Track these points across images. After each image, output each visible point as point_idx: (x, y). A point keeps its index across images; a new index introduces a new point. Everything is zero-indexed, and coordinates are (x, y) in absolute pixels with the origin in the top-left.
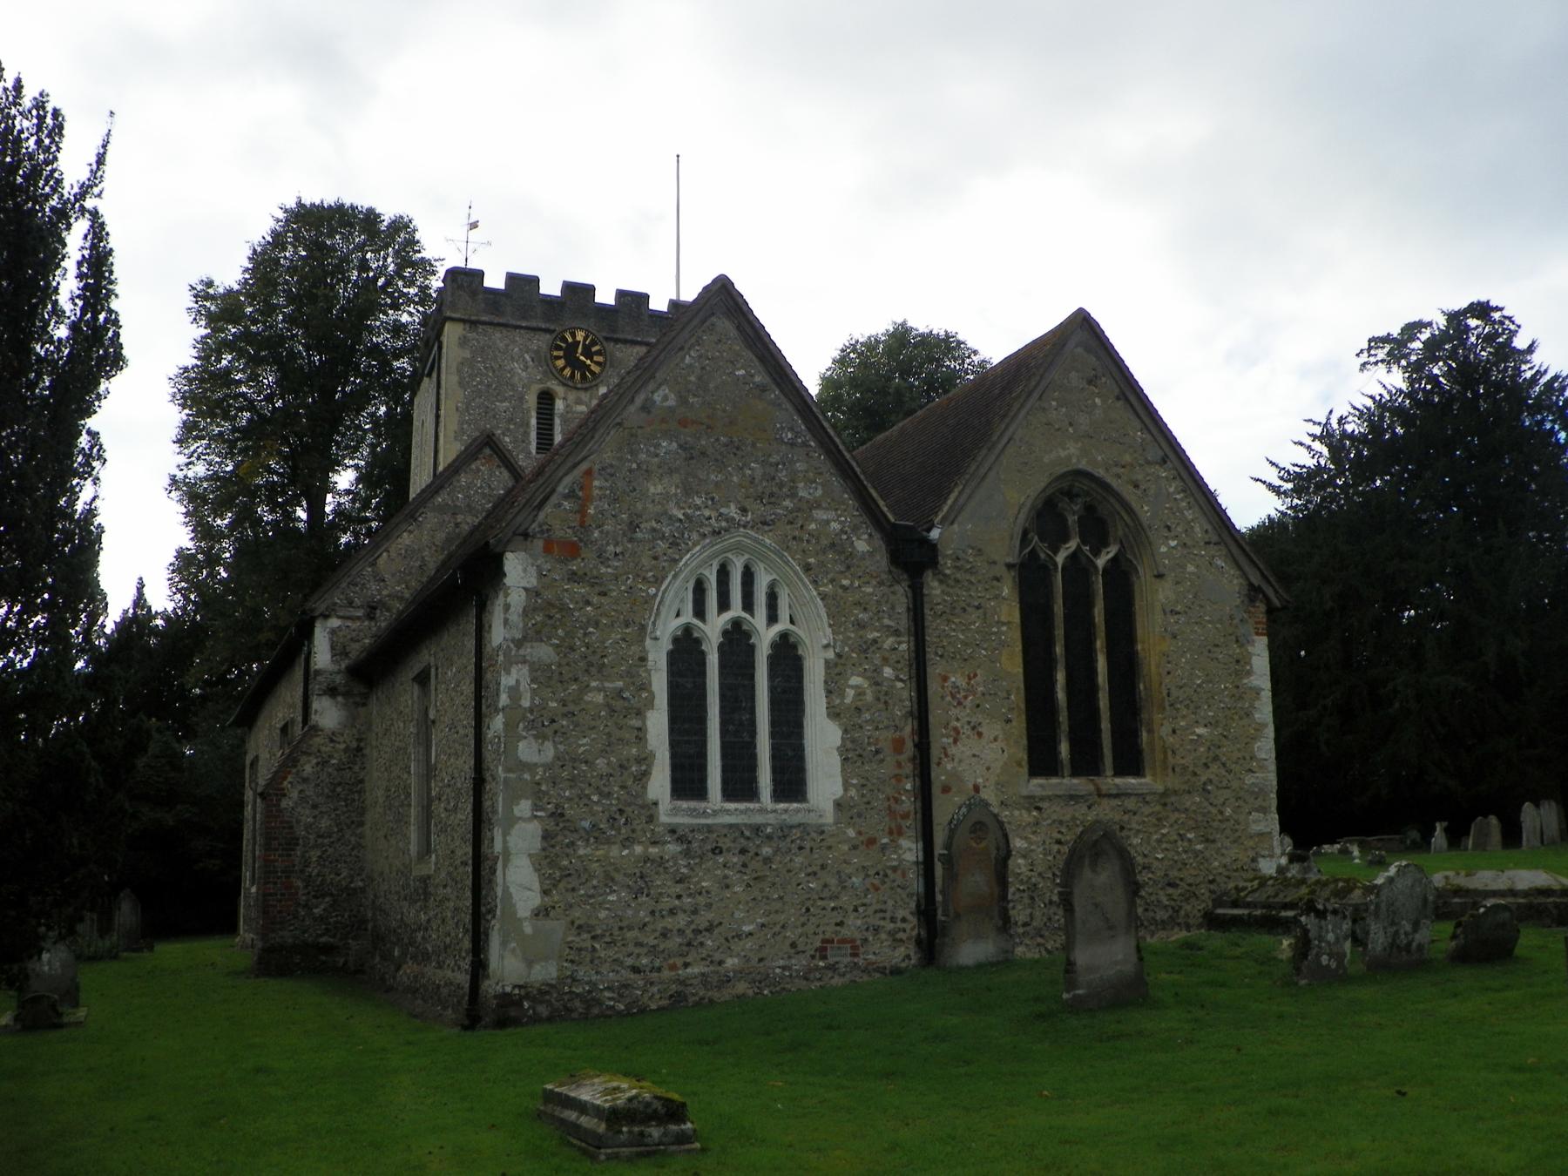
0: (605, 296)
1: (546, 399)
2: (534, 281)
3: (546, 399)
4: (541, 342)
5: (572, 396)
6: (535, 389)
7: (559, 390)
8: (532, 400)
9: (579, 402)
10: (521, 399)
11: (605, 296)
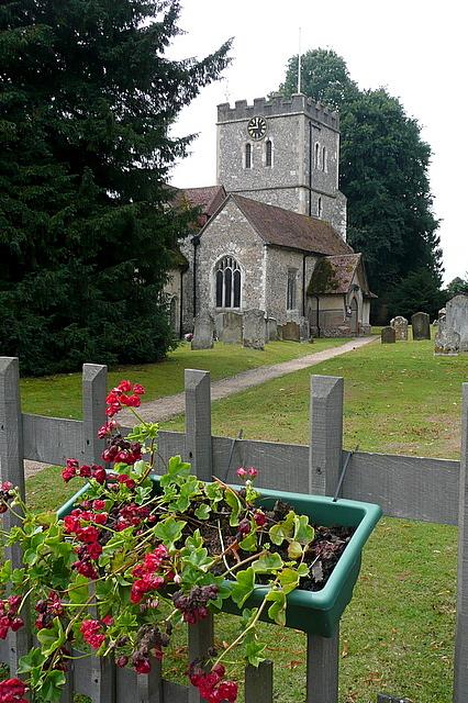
0: (250, 103)
1: (248, 146)
2: (245, 102)
3: (248, 146)
8: (243, 148)
11: (250, 103)
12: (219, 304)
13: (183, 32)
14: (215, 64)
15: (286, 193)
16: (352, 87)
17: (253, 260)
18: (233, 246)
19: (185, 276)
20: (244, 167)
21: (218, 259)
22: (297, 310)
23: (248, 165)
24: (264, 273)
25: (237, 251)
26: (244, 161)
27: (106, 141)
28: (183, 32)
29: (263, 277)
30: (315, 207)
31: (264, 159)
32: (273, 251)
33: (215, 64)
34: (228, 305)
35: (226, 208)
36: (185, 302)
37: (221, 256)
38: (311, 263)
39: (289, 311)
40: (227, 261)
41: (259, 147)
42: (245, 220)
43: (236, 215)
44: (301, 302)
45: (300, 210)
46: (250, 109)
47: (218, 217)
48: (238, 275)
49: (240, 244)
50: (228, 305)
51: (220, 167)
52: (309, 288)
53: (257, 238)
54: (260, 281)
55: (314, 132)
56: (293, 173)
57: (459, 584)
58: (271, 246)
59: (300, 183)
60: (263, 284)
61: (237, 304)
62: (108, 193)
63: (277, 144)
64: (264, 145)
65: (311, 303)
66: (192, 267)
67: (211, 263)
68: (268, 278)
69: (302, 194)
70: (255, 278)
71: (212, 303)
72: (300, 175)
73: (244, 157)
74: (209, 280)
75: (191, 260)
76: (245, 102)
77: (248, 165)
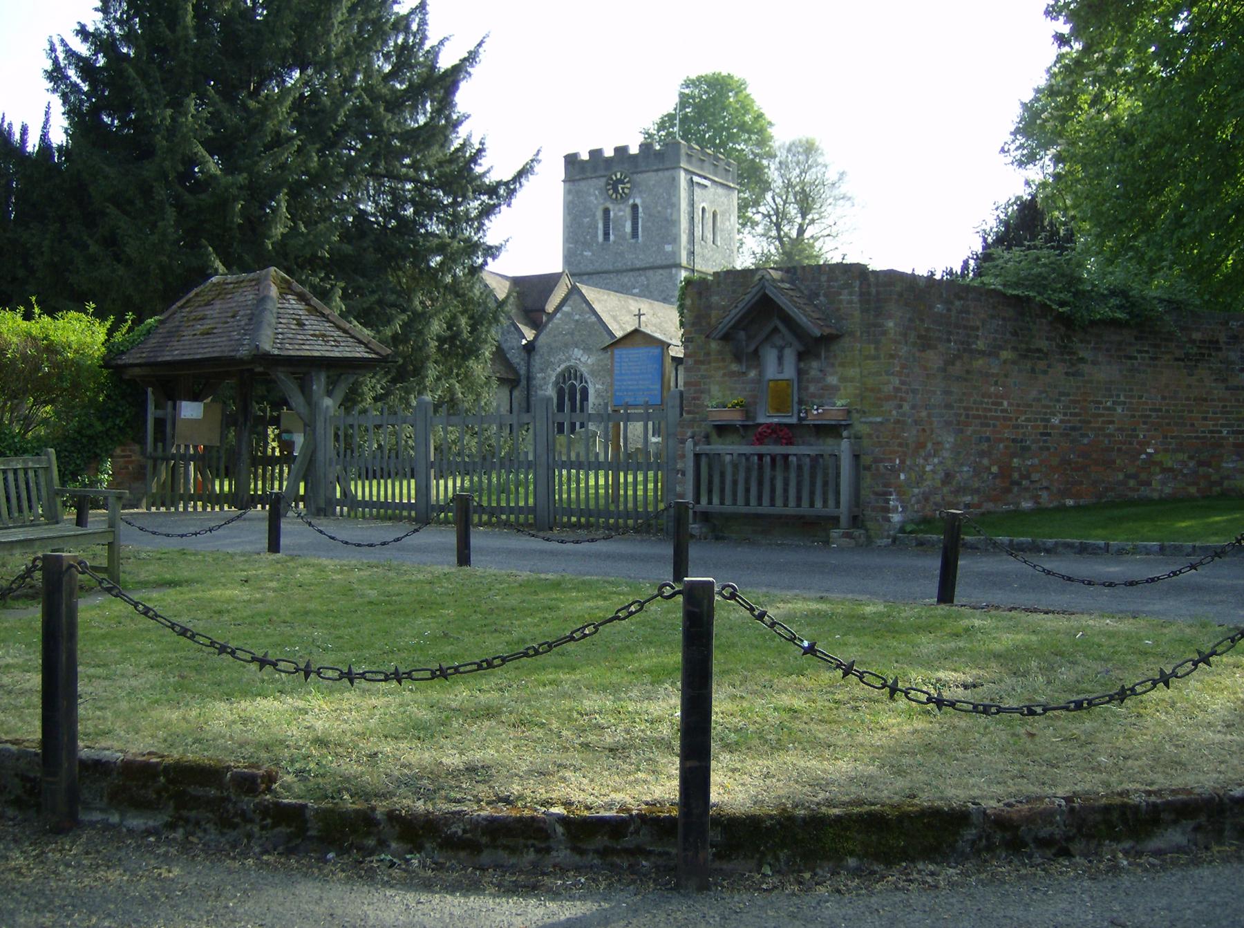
0: (585, 156)
1: (606, 212)
3: (606, 212)
4: (602, 181)
5: (617, 208)
6: (601, 208)
7: (611, 206)
8: (599, 214)
9: (620, 210)
10: (594, 215)
14: (24, 131)
16: (1071, 71)
18: (577, 353)
19: (516, 393)
20: (601, 238)
21: (559, 370)
23: (606, 234)
27: (455, 186)
31: (628, 228)
33: (24, 131)
35: (569, 302)
37: (563, 366)
40: (571, 374)
41: (621, 212)
46: (609, 161)
47: (559, 315)
48: (585, 392)
49: (587, 350)
55: (697, 190)
57: (957, 590)
62: (438, 259)
63: (646, 208)
64: (628, 210)
66: (524, 382)
67: (549, 376)
73: (601, 226)
75: (523, 372)
77: (606, 234)
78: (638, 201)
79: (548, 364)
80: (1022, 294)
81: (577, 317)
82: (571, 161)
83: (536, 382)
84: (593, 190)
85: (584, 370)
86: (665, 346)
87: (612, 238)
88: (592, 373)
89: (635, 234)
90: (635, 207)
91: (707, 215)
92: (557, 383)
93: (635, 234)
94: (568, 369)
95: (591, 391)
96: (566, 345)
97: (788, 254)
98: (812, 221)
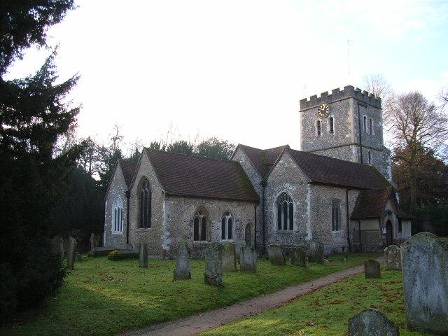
1: (319, 122)
2: (327, 92)
3: (319, 122)
8: (315, 124)
12: (280, 228)
13: (75, 111)
15: (343, 150)
17: (301, 195)
18: (287, 185)
19: (258, 208)
20: (317, 135)
22: (341, 232)
23: (319, 133)
24: (309, 204)
25: (290, 189)
26: (316, 132)
28: (75, 111)
29: (308, 207)
30: (365, 157)
32: (316, 187)
34: (285, 228)
36: (258, 226)
37: (280, 193)
38: (353, 196)
39: (334, 232)
40: (284, 197)
42: (295, 166)
43: (289, 163)
44: (346, 224)
45: (354, 160)
47: (277, 165)
48: (291, 206)
49: (292, 183)
50: (285, 228)
51: (303, 137)
52: (353, 213)
53: (303, 177)
54: (306, 210)
55: (362, 109)
56: (347, 136)
58: (314, 183)
59: (353, 142)
60: (308, 213)
61: (291, 228)
65: (354, 225)
68: (312, 208)
69: (354, 149)
70: (303, 209)
71: (275, 227)
72: (353, 137)
74: (273, 210)
75: (261, 197)
76: (327, 92)
77: (319, 133)
78: (333, 116)
79: (273, 192)
80: (91, 178)
81: (286, 166)
82: (303, 102)
83: (268, 202)
84: (315, 118)
85: (290, 194)
86: (390, 152)
87: (321, 134)
88: (294, 195)
89: (332, 131)
90: (331, 119)
91: (367, 121)
92: (277, 202)
93: (332, 131)
94: (283, 194)
95: (294, 206)
96: (281, 182)
97: (410, 143)
98: (419, 129)
